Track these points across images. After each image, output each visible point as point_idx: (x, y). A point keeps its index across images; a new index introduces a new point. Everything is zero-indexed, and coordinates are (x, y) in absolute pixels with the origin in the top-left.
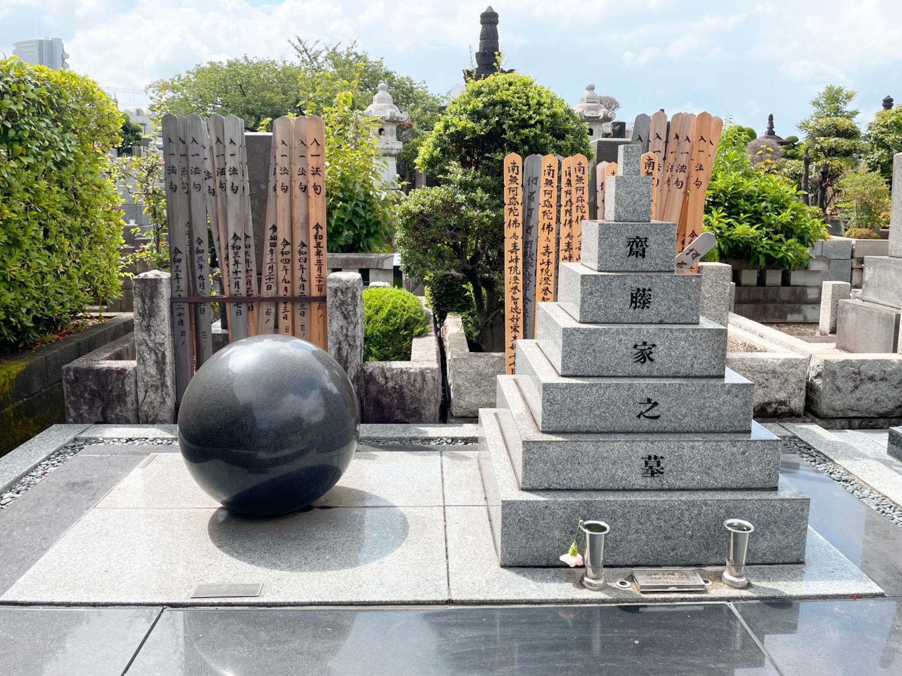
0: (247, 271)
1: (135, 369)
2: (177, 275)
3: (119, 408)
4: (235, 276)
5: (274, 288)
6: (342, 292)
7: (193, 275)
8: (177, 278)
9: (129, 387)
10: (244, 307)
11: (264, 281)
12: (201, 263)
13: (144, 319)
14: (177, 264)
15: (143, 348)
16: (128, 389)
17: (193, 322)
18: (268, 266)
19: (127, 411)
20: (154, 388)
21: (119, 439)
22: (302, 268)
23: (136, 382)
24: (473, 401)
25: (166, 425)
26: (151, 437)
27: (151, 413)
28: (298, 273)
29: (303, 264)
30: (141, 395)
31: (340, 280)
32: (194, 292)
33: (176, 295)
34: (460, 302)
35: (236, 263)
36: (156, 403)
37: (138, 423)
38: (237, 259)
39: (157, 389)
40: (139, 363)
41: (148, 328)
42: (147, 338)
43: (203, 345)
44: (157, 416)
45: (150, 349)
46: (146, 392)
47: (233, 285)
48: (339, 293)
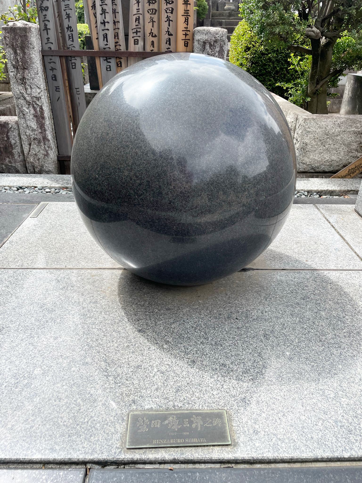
0: (114, 23)
1: (17, 123)
2: (46, 25)
3: (7, 160)
4: (103, 27)
5: (141, 43)
6: (211, 45)
7: (61, 25)
8: (46, 29)
9: (14, 140)
10: (113, 62)
11: (131, 35)
12: (68, 11)
13: (18, 72)
14: (44, 13)
15: (22, 101)
16: (13, 142)
17: (66, 77)
18: (134, 18)
19: (15, 162)
20: (36, 142)
21: (10, 187)
22: (169, 20)
23: (19, 135)
24: (316, 158)
25: (52, 175)
26: (39, 186)
27: (36, 164)
28: (165, 26)
29: (170, 15)
30: (26, 149)
31: (208, 32)
32: (64, 46)
33: (46, 48)
34: (270, 80)
35: (104, 12)
36: (41, 156)
37: (27, 173)
38: (105, 7)
39: (39, 142)
40: (19, 117)
41: (23, 81)
42: (23, 91)
43: (78, 101)
44: (42, 166)
45: (29, 103)
46: (30, 145)
47: (101, 38)
48: (207, 47)
